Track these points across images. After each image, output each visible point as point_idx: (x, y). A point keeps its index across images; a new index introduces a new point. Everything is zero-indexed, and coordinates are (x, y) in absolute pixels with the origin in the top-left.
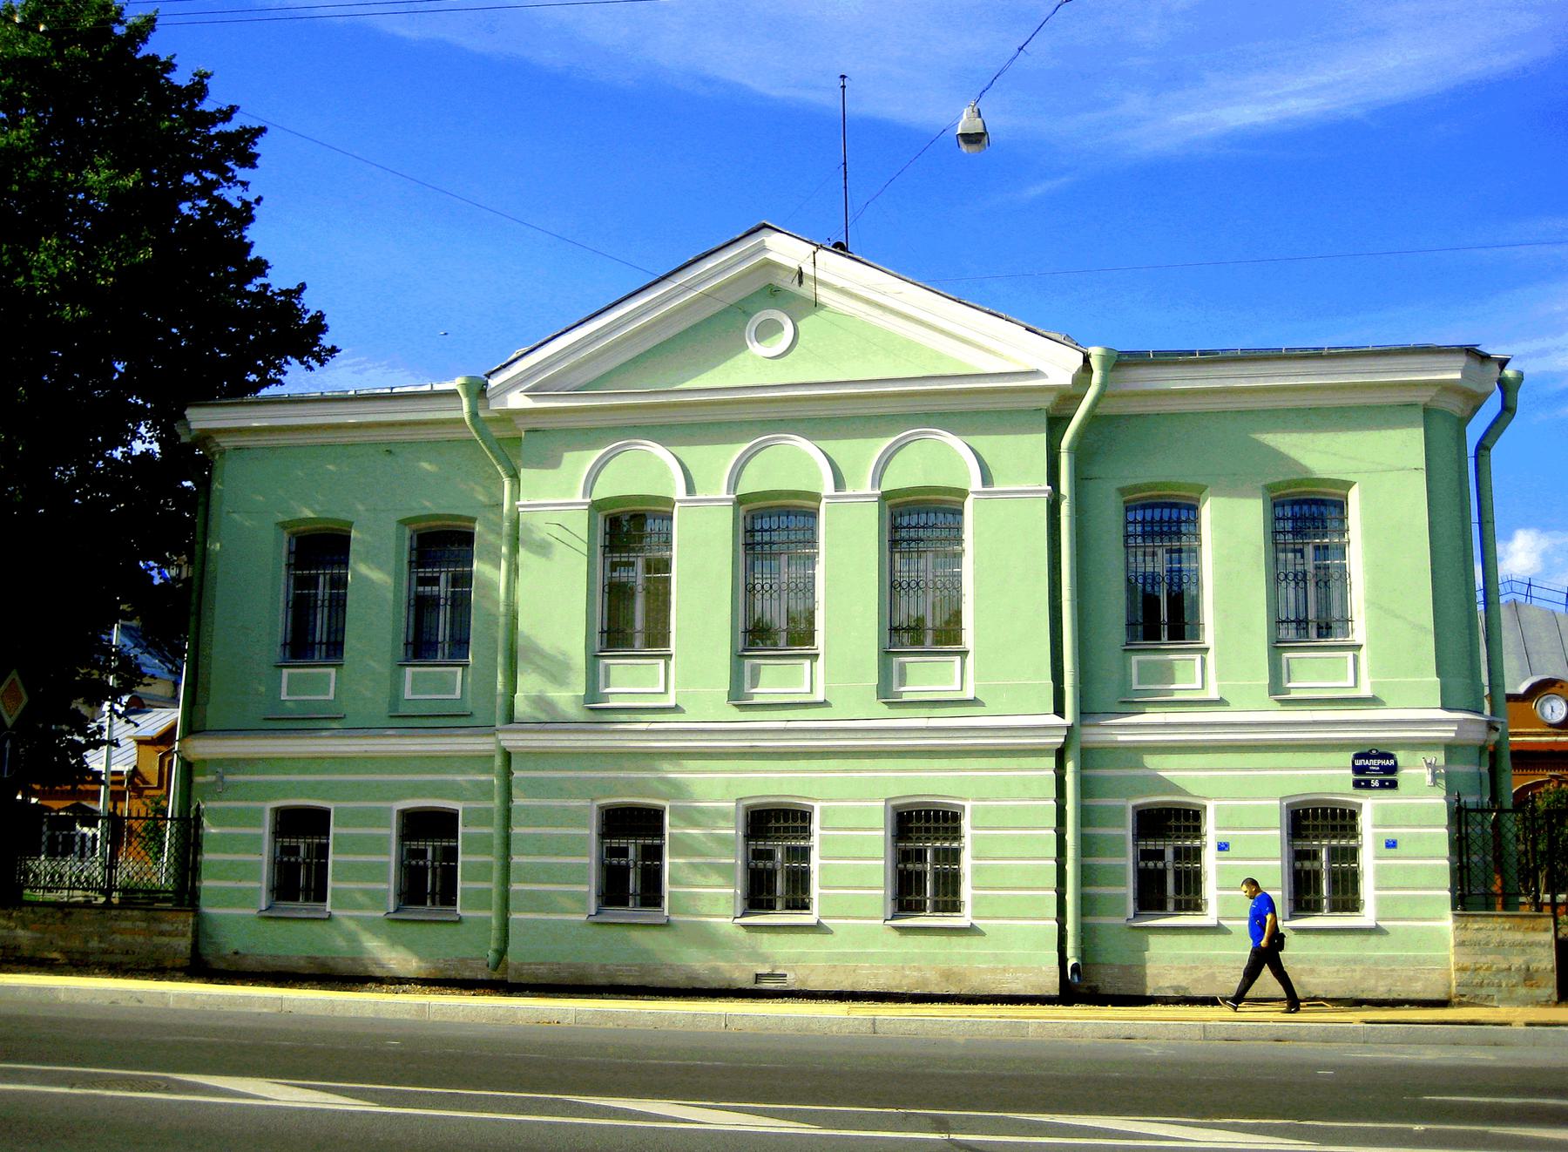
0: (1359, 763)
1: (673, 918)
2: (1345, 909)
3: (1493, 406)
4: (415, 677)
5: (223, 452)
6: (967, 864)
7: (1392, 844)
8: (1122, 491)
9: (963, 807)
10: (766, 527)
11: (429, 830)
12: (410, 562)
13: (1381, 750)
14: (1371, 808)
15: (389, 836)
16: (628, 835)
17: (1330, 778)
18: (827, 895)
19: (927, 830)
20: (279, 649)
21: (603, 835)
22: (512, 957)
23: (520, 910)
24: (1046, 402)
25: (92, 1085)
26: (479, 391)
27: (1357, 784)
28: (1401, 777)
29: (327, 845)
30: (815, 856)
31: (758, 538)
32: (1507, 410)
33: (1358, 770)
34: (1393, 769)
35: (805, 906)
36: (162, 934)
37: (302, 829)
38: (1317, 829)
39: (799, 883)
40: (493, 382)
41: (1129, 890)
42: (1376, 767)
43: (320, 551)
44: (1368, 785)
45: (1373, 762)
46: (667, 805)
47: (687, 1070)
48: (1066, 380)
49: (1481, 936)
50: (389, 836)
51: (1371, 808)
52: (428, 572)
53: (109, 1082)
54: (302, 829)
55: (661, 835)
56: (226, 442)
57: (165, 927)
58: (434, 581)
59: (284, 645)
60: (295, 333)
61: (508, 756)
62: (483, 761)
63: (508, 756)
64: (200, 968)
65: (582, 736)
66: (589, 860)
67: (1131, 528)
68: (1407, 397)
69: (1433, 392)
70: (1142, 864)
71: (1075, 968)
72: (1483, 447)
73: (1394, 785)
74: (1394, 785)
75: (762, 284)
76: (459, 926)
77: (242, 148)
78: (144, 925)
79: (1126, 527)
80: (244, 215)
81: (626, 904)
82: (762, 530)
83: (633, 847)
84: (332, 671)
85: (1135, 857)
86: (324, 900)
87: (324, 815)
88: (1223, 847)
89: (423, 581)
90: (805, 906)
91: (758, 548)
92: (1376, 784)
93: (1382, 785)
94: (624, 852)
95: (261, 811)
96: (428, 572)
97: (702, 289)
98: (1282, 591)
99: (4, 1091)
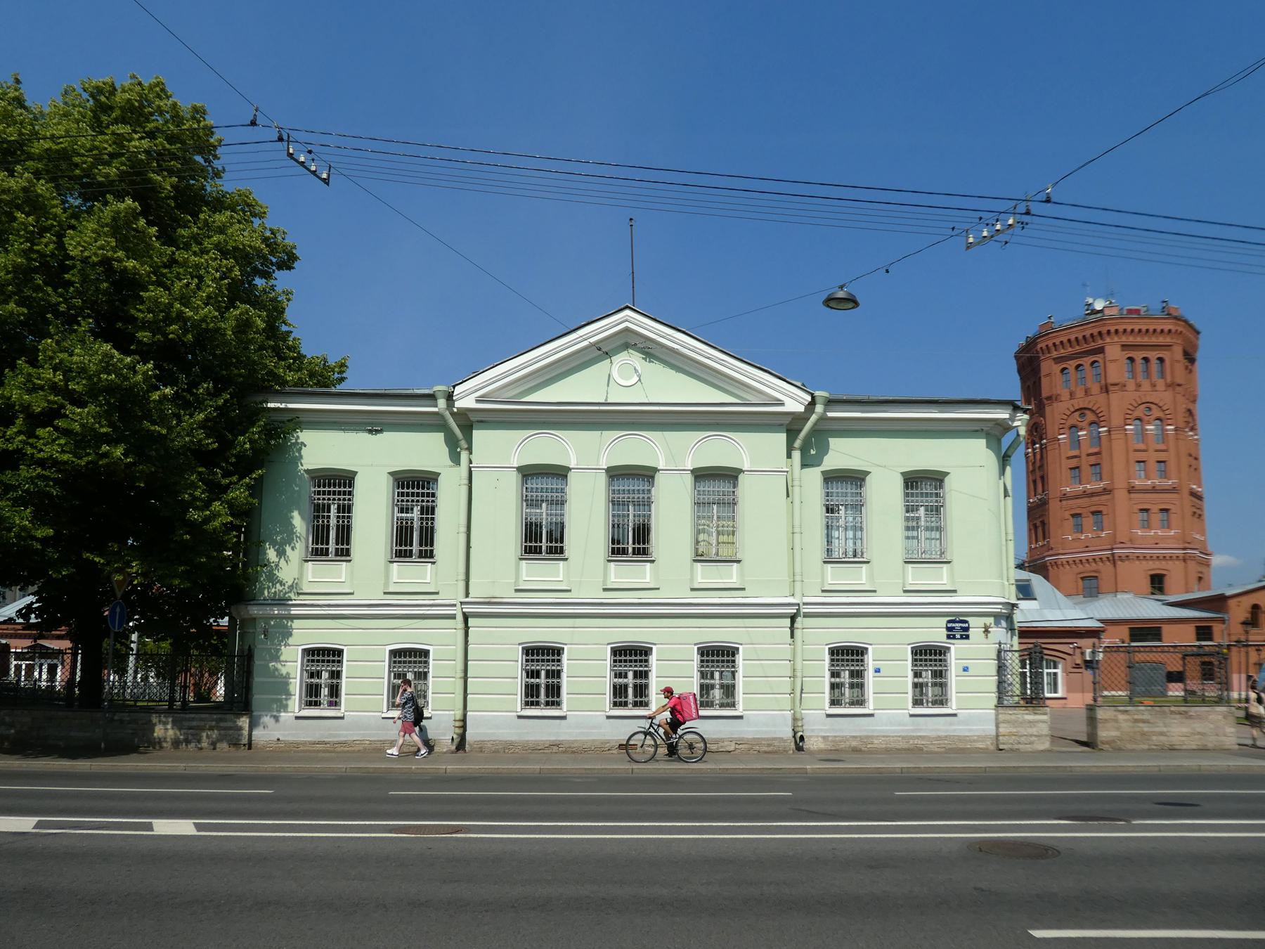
6: (565, 681)
7: (966, 669)
9: (949, 648)
14: (957, 650)
17: (935, 633)
24: (787, 420)
26: (450, 397)
27: (949, 637)
30: (564, 675)
33: (949, 629)
34: (967, 629)
35: (646, 705)
39: (554, 692)
40: (458, 390)
42: (958, 628)
44: (954, 638)
47: (312, 780)
48: (801, 409)
51: (957, 650)
69: (990, 425)
73: (967, 637)
74: (967, 637)
75: (622, 342)
76: (563, 722)
87: (339, 653)
88: (878, 671)
90: (646, 705)
93: (962, 638)
97: (592, 340)
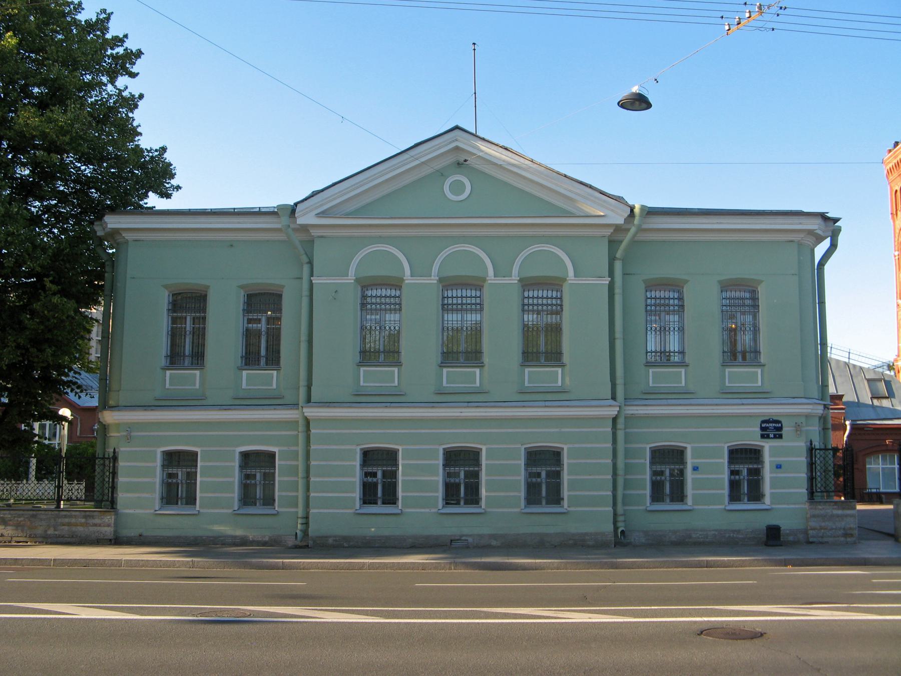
0: (763, 425)
1: (201, 511)
2: (472, 503)
3: (826, 244)
4: (249, 377)
5: (127, 242)
7: (779, 467)
8: (645, 281)
10: (535, 296)
11: (257, 463)
12: (244, 310)
13: (775, 418)
15: (723, 463)
16: (378, 465)
18: (407, 497)
19: (751, 458)
20: (358, 354)
21: (527, 465)
22: (312, 532)
23: (314, 508)
25: (691, 615)
27: (763, 436)
28: (784, 432)
29: (196, 472)
31: (369, 300)
32: (833, 246)
33: (762, 429)
34: (780, 429)
36: (95, 525)
37: (179, 462)
38: (745, 458)
41: (648, 492)
42: (772, 428)
43: (189, 303)
44: (768, 437)
45: (771, 425)
46: (400, 448)
49: (822, 512)
50: (723, 463)
52: (254, 316)
53: (690, 614)
54: (179, 462)
55: (397, 465)
56: (128, 236)
57: (97, 521)
58: (259, 321)
59: (166, 357)
60: (157, 174)
61: (307, 422)
62: (293, 424)
63: (307, 422)
64: (117, 541)
65: (500, 410)
66: (157, 479)
67: (526, 301)
68: (790, 237)
70: (654, 478)
71: (623, 532)
72: (822, 264)
73: (780, 437)
74: (780, 437)
77: (125, 63)
78: (83, 520)
79: (646, 301)
80: (132, 103)
81: (376, 503)
82: (528, 298)
83: (744, 469)
84: (197, 372)
85: (444, 476)
86: (195, 504)
88: (695, 469)
89: (250, 321)
91: (369, 306)
92: (772, 436)
93: (775, 437)
94: (374, 475)
95: (155, 452)
96: (254, 316)
98: (549, 337)
99: (1, 618)
